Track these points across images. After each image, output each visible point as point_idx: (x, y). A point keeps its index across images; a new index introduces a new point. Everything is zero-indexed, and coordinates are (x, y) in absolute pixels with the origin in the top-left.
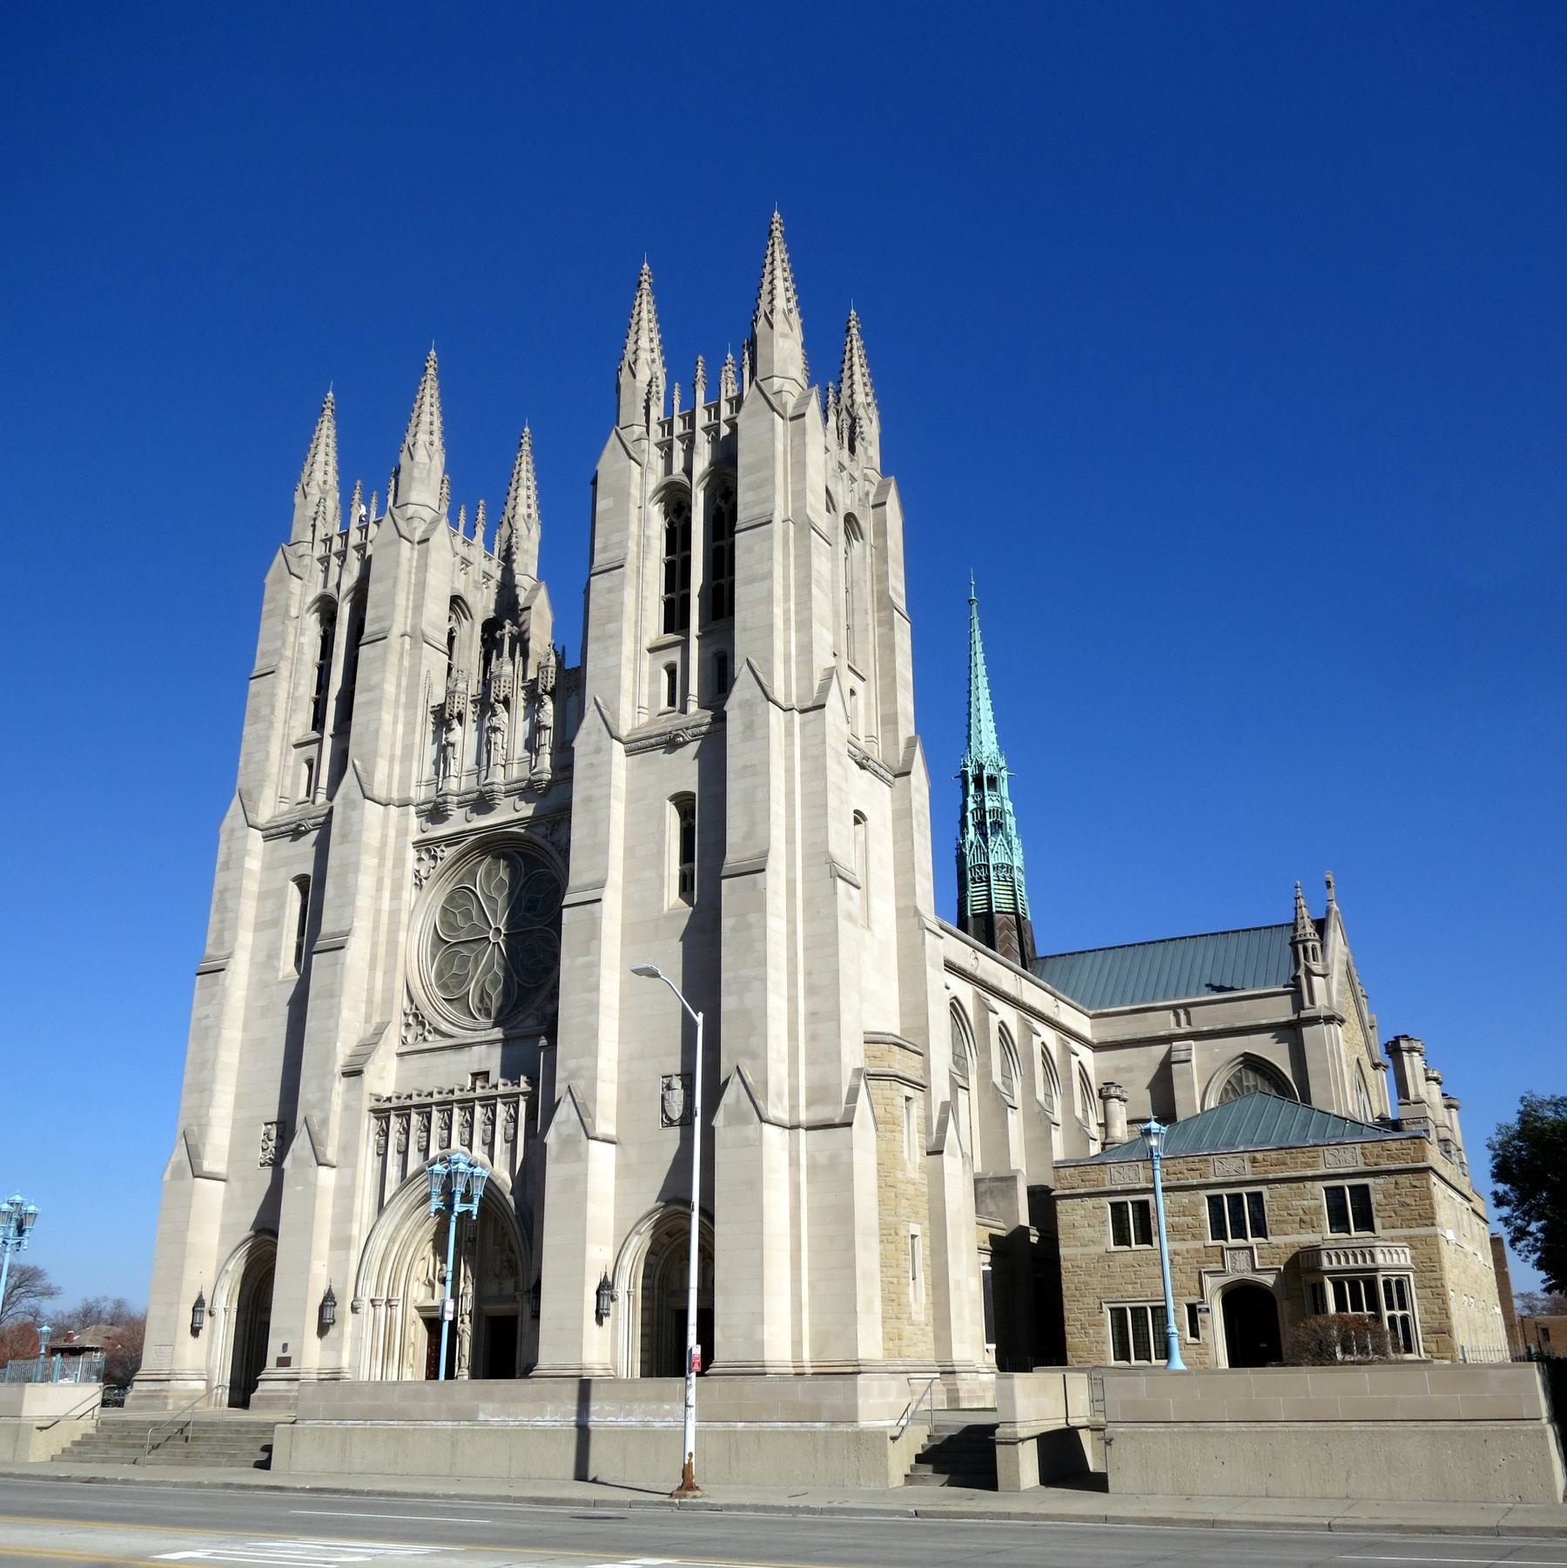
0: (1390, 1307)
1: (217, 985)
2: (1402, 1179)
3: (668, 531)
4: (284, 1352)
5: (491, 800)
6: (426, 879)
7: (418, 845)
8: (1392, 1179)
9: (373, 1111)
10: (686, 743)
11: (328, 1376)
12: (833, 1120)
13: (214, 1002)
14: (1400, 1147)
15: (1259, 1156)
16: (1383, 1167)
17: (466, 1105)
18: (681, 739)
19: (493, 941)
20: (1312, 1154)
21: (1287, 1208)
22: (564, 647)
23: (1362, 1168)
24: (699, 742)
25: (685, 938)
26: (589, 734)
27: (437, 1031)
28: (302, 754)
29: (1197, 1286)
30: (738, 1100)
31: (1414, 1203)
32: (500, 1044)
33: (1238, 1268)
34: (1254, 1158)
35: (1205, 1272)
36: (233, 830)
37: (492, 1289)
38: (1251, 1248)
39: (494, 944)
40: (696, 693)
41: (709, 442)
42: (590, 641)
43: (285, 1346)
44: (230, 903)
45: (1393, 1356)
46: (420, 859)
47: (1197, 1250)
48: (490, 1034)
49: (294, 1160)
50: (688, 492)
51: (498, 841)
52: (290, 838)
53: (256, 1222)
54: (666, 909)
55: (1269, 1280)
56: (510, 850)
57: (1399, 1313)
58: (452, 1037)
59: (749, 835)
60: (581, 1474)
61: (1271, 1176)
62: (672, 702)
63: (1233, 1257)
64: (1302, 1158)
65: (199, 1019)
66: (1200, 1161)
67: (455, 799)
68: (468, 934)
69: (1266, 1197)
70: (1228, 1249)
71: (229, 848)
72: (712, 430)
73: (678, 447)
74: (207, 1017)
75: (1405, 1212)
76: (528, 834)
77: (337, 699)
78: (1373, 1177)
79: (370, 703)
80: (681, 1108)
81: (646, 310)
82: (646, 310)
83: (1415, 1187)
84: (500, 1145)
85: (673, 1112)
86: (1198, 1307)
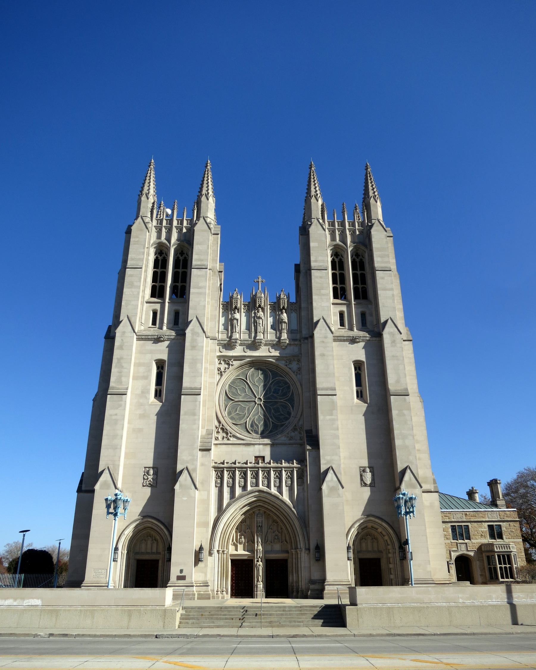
0: (500, 563)
1: (122, 401)
2: (511, 523)
3: (155, 260)
5: (234, 346)
6: (224, 372)
7: (219, 357)
8: (508, 523)
9: (214, 467)
12: (431, 490)
13: (120, 408)
14: (510, 513)
15: (468, 513)
16: (505, 519)
17: (266, 469)
20: (484, 514)
21: (477, 531)
22: (289, 293)
23: (499, 519)
24: (169, 342)
25: (365, 415)
26: (321, 330)
27: (234, 436)
28: (150, 306)
29: (449, 555)
30: (410, 479)
31: (514, 531)
33: (462, 551)
34: (466, 514)
35: (452, 551)
37: (269, 548)
38: (466, 543)
39: (258, 404)
40: (166, 323)
41: (156, 232)
43: (181, 571)
44: (125, 365)
45: (501, 580)
46: (220, 363)
47: (449, 543)
48: (264, 441)
49: (181, 486)
50: (168, 249)
52: (153, 342)
54: (150, 402)
55: (472, 554)
56: (264, 367)
57: (503, 566)
58: (243, 440)
60: (515, 622)
61: (472, 520)
62: (154, 323)
63: (460, 546)
64: (481, 515)
65: (111, 415)
68: (243, 398)
69: (470, 527)
70: (459, 543)
71: (122, 340)
72: (180, 230)
73: (164, 230)
74: (116, 415)
75: (512, 534)
76: (277, 363)
78: (503, 522)
80: (370, 480)
83: (515, 526)
84: (285, 489)
85: (367, 480)
86: (450, 562)
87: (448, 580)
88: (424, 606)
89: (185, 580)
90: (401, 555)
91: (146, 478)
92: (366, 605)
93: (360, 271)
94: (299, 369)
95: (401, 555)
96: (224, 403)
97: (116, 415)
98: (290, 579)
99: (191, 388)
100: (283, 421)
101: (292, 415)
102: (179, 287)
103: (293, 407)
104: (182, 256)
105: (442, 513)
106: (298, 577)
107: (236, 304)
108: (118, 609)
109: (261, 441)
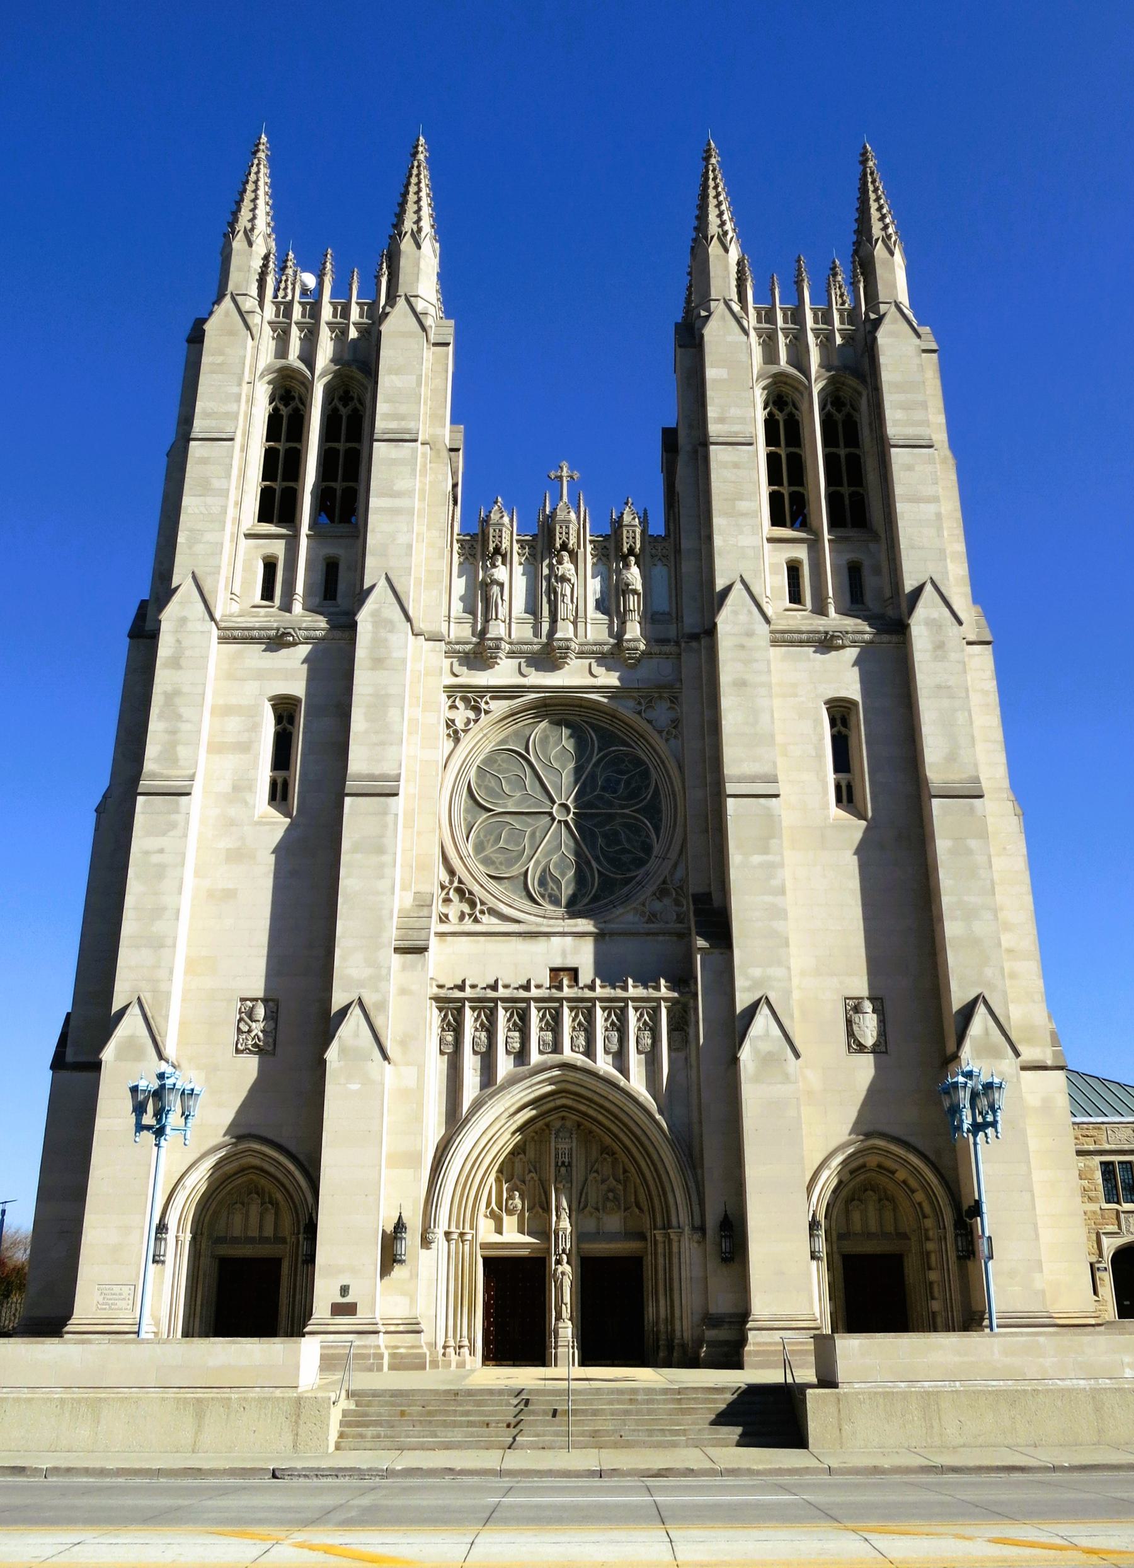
4: (343, 1296)
9: (437, 999)
10: (843, 647)
11: (401, 1328)
18: (291, 639)
19: (558, 818)
22: (645, 510)
24: (310, 647)
25: (858, 851)
26: (735, 613)
27: (492, 912)
30: (986, 1030)
32: (591, 939)
35: (1104, 1233)
36: (183, 621)
37: (590, 1226)
42: (681, 516)
43: (344, 1290)
46: (453, 707)
47: (1094, 1212)
48: (576, 926)
49: (343, 1051)
50: (308, 386)
51: (561, 705)
52: (264, 646)
53: (857, 1123)
59: (952, 758)
63: (1127, 1220)
65: (147, 853)
66: (1095, 1128)
67: (508, 646)
70: (1123, 1212)
71: (178, 641)
72: (339, 331)
74: (161, 851)
76: (614, 705)
77: (312, 493)
79: (395, 511)
80: (875, 1034)
81: (262, 177)
82: (262, 177)
85: (864, 1036)
87: (1093, 1315)
88: (1026, 1388)
89: (355, 1315)
90: (960, 1244)
91: (245, 1028)
92: (863, 1385)
93: (849, 486)
94: (676, 723)
95: (960, 1244)
96: (465, 820)
97: (161, 851)
98: (650, 1311)
99: (373, 778)
100: (629, 870)
101: (655, 853)
102: (339, 493)
103: (657, 829)
104: (345, 406)
105: (1076, 1127)
106: (672, 1306)
107: (497, 542)
108: (166, 1395)
109: (569, 926)
